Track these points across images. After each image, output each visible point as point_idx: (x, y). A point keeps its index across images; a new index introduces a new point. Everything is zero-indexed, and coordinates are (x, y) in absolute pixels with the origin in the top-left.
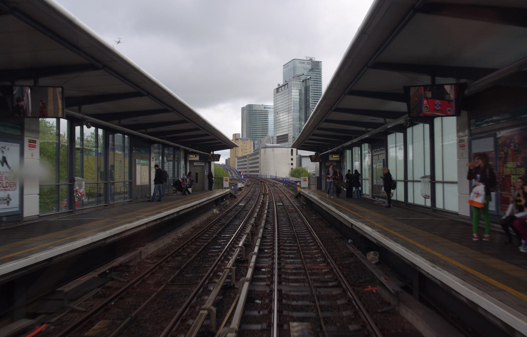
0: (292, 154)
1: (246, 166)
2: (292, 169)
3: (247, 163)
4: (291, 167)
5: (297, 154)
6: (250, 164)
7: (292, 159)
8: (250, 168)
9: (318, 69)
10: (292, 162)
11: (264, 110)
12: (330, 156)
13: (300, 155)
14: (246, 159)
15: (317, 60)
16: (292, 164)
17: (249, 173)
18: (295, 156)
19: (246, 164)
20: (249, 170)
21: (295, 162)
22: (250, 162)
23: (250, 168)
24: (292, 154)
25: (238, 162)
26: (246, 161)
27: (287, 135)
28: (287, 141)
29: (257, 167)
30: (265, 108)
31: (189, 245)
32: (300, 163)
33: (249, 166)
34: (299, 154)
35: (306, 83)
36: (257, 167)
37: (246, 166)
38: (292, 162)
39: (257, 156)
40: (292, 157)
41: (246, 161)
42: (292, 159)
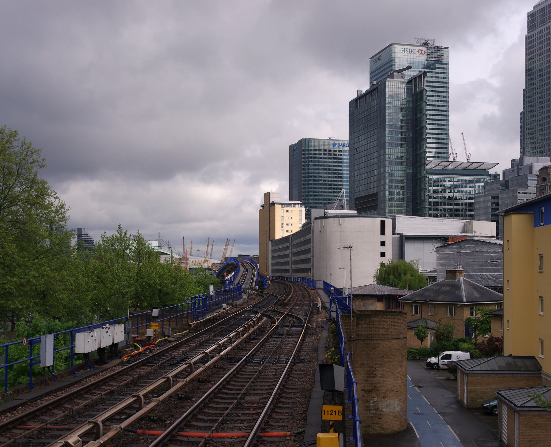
0: (383, 232)
1: (288, 259)
2: (382, 264)
3: (288, 252)
4: (383, 259)
5: (394, 232)
6: (295, 254)
7: (383, 244)
8: (295, 262)
9: (441, 63)
10: (382, 249)
11: (333, 148)
12: (343, 369)
13: (401, 235)
14: (288, 244)
15: (437, 44)
16: (383, 254)
17: (294, 275)
18: (389, 237)
19: (287, 256)
20: (294, 267)
21: (389, 250)
22: (294, 250)
23: (295, 262)
24: (383, 232)
25: (273, 251)
26: (287, 248)
27: (377, 193)
28: (384, 221)
29: (307, 261)
30: (334, 145)
31: (207, 404)
32: (401, 254)
33: (294, 259)
34: (398, 231)
35: (416, 86)
36: (307, 261)
37: (288, 259)
38: (382, 249)
39: (308, 237)
40: (383, 238)
41: (287, 248)
42: (383, 244)
